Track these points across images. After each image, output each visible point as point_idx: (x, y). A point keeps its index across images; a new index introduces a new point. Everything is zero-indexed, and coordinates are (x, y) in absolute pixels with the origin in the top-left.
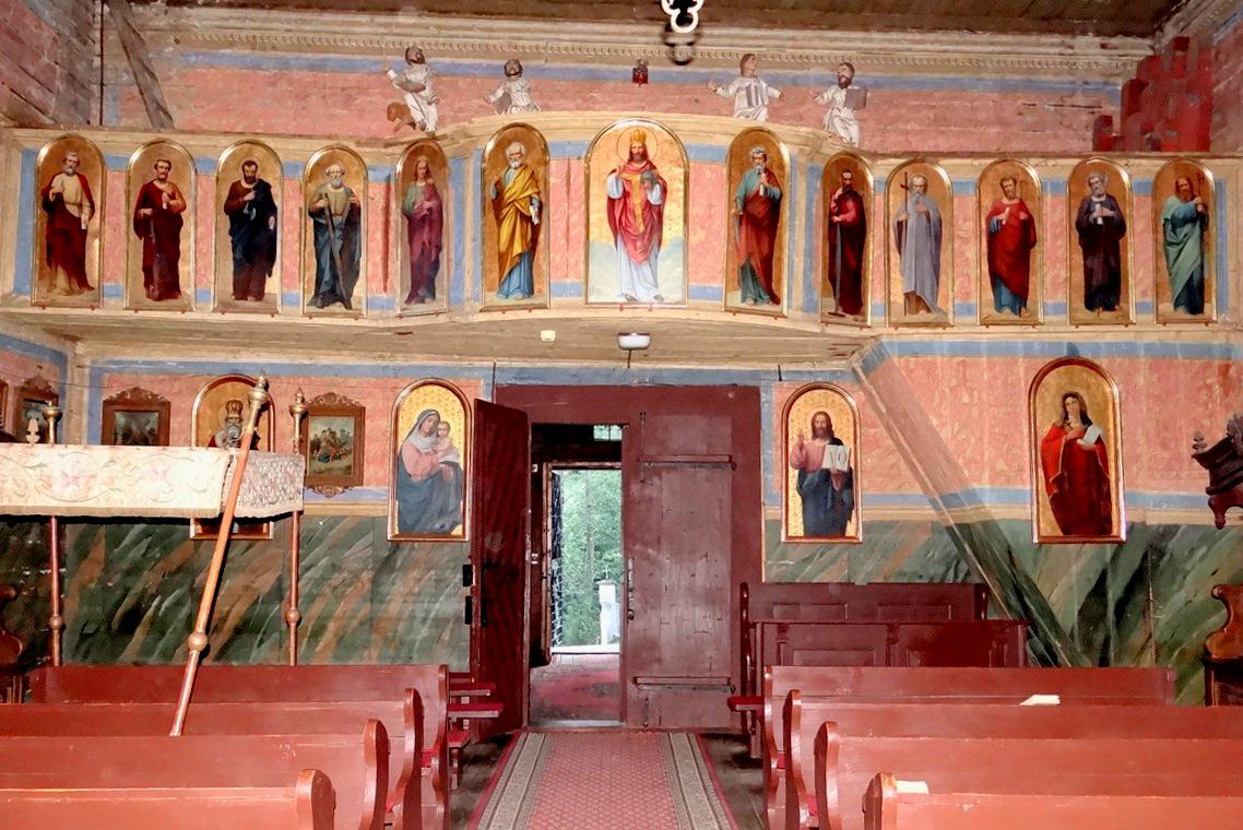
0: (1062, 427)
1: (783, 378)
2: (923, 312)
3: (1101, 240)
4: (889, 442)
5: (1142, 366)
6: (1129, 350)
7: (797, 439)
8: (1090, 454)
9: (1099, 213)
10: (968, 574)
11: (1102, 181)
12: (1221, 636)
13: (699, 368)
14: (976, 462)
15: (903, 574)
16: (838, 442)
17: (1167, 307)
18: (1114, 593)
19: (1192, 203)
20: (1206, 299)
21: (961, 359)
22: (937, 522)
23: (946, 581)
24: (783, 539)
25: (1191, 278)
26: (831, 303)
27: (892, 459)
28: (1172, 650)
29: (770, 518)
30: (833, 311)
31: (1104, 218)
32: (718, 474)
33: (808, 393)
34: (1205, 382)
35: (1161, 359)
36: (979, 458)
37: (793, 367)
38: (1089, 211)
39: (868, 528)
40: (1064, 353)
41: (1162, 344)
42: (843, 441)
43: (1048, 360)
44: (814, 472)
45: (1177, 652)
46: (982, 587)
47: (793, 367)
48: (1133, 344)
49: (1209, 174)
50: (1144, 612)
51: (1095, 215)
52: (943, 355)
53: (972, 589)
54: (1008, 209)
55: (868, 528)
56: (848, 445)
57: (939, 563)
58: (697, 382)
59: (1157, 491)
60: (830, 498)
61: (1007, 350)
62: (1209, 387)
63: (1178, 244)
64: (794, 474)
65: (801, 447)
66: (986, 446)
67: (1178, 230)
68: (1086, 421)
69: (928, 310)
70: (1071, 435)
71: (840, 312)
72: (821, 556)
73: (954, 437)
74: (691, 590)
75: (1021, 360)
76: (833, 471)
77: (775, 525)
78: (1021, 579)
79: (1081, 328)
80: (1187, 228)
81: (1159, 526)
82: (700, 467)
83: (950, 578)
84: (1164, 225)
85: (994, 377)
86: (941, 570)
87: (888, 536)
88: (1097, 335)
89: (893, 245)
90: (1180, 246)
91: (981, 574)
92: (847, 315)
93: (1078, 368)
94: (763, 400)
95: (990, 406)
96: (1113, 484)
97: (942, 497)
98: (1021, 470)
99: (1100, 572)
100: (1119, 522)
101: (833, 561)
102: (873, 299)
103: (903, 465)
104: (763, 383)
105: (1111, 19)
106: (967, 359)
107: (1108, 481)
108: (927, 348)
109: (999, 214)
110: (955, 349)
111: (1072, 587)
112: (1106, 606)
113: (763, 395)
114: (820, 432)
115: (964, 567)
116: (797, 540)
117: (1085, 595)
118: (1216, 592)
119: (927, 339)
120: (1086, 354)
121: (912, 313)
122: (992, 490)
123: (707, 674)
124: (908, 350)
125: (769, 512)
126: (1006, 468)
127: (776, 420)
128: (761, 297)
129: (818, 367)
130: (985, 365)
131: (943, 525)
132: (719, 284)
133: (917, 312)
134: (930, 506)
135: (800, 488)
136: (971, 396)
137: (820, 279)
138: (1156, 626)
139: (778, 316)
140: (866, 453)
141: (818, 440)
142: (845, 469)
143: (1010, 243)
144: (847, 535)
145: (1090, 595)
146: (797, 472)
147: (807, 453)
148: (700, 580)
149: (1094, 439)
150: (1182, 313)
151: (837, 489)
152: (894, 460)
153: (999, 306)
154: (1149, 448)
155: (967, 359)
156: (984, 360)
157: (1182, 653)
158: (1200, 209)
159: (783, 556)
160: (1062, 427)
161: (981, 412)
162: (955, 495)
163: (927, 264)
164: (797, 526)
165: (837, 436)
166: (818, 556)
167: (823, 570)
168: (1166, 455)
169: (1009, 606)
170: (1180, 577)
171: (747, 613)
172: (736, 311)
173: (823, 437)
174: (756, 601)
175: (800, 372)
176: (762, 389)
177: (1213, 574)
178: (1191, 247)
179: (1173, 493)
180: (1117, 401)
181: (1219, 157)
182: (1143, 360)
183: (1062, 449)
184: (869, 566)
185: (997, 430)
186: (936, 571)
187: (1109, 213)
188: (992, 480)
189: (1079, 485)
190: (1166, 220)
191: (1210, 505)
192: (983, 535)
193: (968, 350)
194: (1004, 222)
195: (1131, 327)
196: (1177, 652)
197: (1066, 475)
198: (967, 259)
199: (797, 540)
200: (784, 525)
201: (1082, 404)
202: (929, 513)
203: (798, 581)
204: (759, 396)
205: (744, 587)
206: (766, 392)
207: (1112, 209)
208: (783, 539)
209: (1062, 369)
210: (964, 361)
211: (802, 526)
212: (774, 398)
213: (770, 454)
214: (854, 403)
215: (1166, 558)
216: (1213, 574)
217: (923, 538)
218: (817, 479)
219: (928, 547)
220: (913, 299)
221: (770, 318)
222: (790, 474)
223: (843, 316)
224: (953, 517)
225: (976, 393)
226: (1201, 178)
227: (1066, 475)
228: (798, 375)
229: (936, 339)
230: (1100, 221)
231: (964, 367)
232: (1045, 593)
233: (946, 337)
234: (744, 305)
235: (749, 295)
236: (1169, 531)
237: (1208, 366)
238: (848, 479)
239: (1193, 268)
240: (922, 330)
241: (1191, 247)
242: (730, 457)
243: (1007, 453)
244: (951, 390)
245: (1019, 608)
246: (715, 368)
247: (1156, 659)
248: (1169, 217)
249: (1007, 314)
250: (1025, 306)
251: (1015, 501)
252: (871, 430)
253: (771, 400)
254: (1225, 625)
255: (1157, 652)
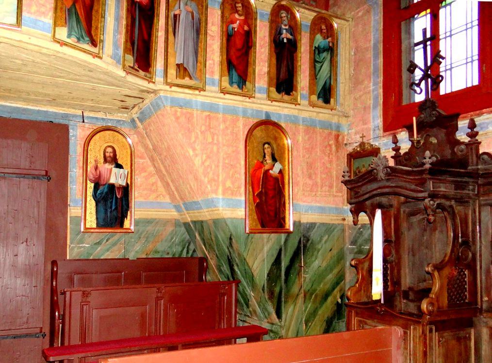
0: (262, 162)
1: (85, 121)
2: (187, 78)
3: (284, 52)
4: (152, 169)
5: (301, 130)
6: (294, 120)
7: (93, 163)
8: (276, 179)
9: (285, 36)
10: (194, 251)
11: (287, 17)
12: (355, 289)
13: (25, 107)
14: (214, 180)
15: (157, 252)
16: (119, 166)
17: (314, 98)
18: (284, 263)
19: (327, 40)
20: (332, 96)
21: (208, 114)
22: (178, 220)
23: (182, 256)
24: (82, 230)
25: (325, 83)
26: (130, 60)
27: (152, 180)
28: (311, 294)
29: (73, 215)
30: (132, 65)
31: (288, 39)
32: (36, 183)
33: (102, 133)
34: (328, 143)
35: (310, 127)
36: (216, 178)
37: (92, 115)
38: (280, 34)
39: (137, 223)
40: (264, 118)
41: (311, 119)
42: (124, 166)
43: (256, 121)
44: (104, 185)
45: (313, 296)
46: (203, 260)
47: (92, 115)
48: (297, 116)
49: (335, 25)
50: (299, 274)
51: (283, 36)
52: (197, 110)
53: (198, 260)
54: (238, 22)
55: (137, 223)
56: (126, 170)
57: (178, 245)
58: (23, 117)
59: (315, 201)
60: (114, 204)
61: (232, 111)
62: (330, 146)
63: (321, 62)
64: (91, 186)
65: (96, 168)
66: (220, 171)
67: (321, 54)
68: (274, 160)
69: (191, 78)
70: (267, 167)
71: (136, 67)
72: (107, 241)
73: (203, 163)
74: (14, 266)
75: (241, 118)
76: (116, 185)
77: (77, 220)
78: (235, 256)
79: (274, 103)
80: (325, 54)
81: (307, 223)
82: (24, 177)
83: (184, 255)
84: (315, 50)
85: (226, 127)
86: (180, 249)
87: (150, 228)
88: (280, 110)
89: (171, 29)
90: (322, 63)
91: (202, 251)
92: (141, 71)
93: (271, 127)
94: (71, 134)
95: (224, 145)
96: (287, 198)
97: (185, 204)
98: (239, 187)
99: (278, 250)
100: (289, 220)
101: (115, 244)
102: (159, 64)
103: (159, 184)
104: (71, 123)
105: (81, 139)
106: (211, 114)
107: (284, 196)
108: (187, 104)
109: (233, 24)
110: (206, 107)
111: (264, 260)
112: (281, 270)
113: (71, 131)
114: (108, 159)
115: (192, 247)
116: (92, 231)
117: (270, 264)
118: (353, 263)
119: (188, 97)
120: (274, 119)
121: (180, 78)
122: (223, 199)
123: (25, 326)
124: (175, 102)
125: (74, 211)
126: (231, 186)
127: (80, 150)
128: (83, 38)
129: (109, 117)
130: (221, 120)
131: (182, 221)
132: (49, 20)
133: (184, 78)
134: (174, 210)
135: (95, 196)
136: (213, 139)
137: (123, 40)
138: (304, 281)
139: (97, 56)
140: (138, 175)
141: (107, 164)
142: (124, 184)
143: (239, 42)
144: (124, 227)
145: (273, 265)
146: (93, 185)
147: (100, 172)
148: (21, 259)
149: (278, 171)
150: (320, 102)
151: (119, 197)
152: (154, 181)
153: (231, 83)
154: (303, 178)
155: (211, 114)
156: (220, 116)
157: (316, 296)
158: (331, 45)
159: (81, 241)
160: (262, 162)
161: (218, 149)
162: (196, 203)
163: (191, 49)
164: (91, 221)
165: (120, 162)
166: (105, 241)
167: (108, 250)
168: (310, 182)
169: (220, 271)
170: (315, 253)
171: (56, 281)
172: (63, 44)
173: (110, 162)
174: (62, 272)
175: (97, 118)
176: (70, 127)
177: (331, 250)
178: (326, 66)
179: (314, 204)
180: (290, 149)
181: (339, 18)
182: (301, 127)
183: (262, 175)
184: (138, 247)
185: (227, 161)
186: (176, 250)
187: (290, 37)
188: (224, 193)
189: (269, 200)
190: (315, 47)
191: (351, 211)
192: (213, 228)
193: (212, 108)
194: (236, 29)
195: (298, 107)
196: (313, 296)
197: (263, 191)
198: (213, 50)
199: (92, 231)
200: (83, 221)
201: (273, 149)
202: (174, 214)
203: (91, 258)
204: (68, 130)
205: (54, 263)
206: (73, 129)
207: (291, 35)
208: (82, 230)
209: (263, 127)
210: (209, 115)
211: (95, 222)
212: (78, 133)
213: (75, 172)
214: (130, 142)
215: (310, 242)
216: (331, 250)
217: (170, 229)
218: (106, 190)
219: (173, 234)
220: (182, 69)
221: (90, 56)
222: (88, 186)
223: (138, 71)
224: (190, 217)
225: (215, 137)
226: (332, 26)
227: (263, 191)
228: (95, 120)
229: (194, 98)
230: (285, 41)
231: (210, 119)
232: (250, 264)
233: (198, 98)
234: (69, 41)
235: (73, 33)
236: (312, 226)
237: (330, 134)
238: (126, 190)
239: (326, 78)
240: (187, 91)
241: (326, 66)
242: (47, 172)
243: (232, 176)
244: (202, 132)
245: (228, 272)
246: (37, 108)
247: (304, 300)
248: (317, 46)
249: (235, 88)
250: (245, 85)
251: (231, 206)
252: (140, 160)
253: (77, 135)
254: (357, 283)
255: (305, 296)
